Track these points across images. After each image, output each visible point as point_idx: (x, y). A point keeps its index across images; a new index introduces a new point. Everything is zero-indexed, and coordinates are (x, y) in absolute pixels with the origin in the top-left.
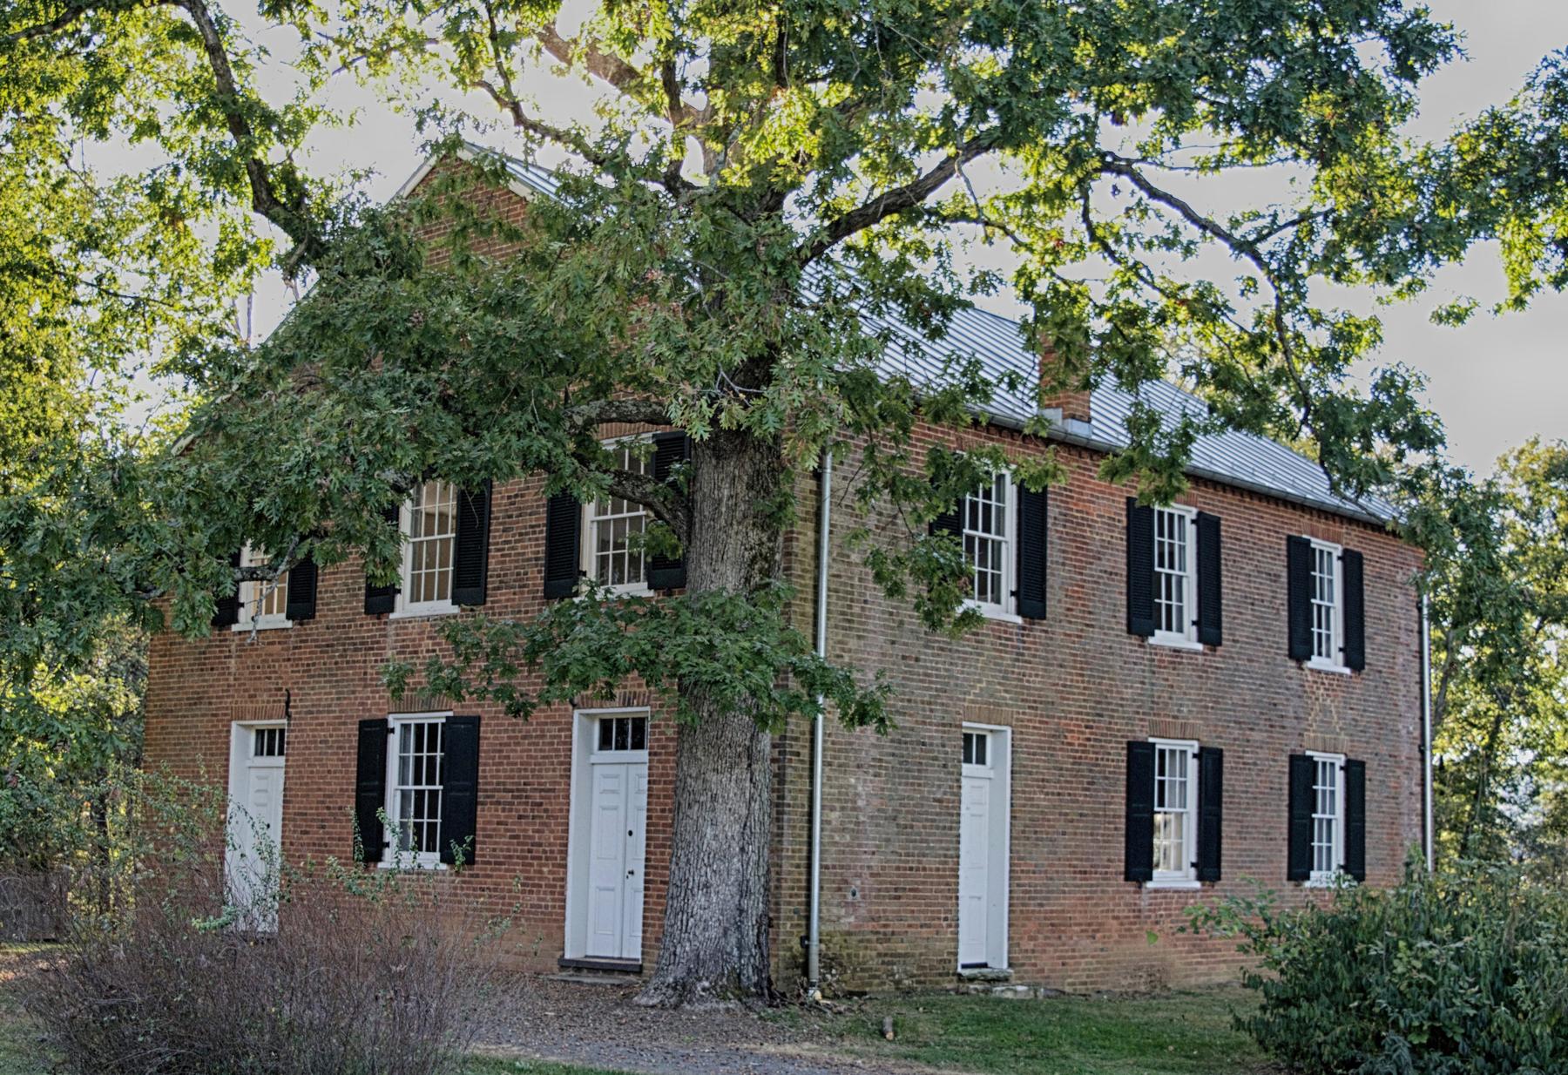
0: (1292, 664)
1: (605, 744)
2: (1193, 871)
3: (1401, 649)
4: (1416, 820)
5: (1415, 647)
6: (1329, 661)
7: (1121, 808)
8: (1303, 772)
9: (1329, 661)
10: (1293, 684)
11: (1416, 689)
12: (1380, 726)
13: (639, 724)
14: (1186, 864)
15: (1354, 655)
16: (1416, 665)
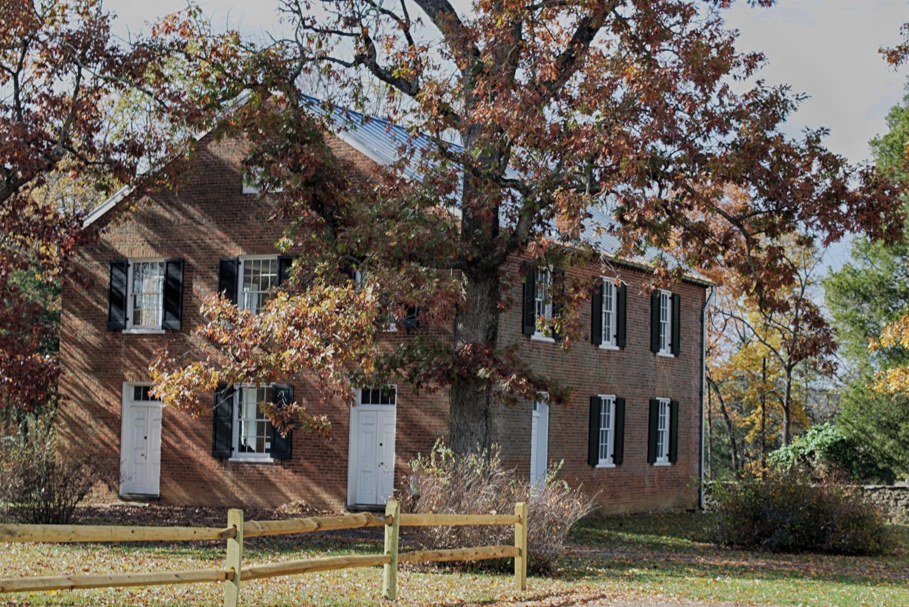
0: (652, 354)
1: (137, 398)
2: (612, 459)
3: (694, 343)
4: (697, 430)
5: (699, 342)
6: (665, 352)
7: (587, 429)
8: (654, 406)
9: (665, 352)
10: (652, 364)
11: (699, 363)
14: (608, 455)
15: (675, 347)
16: (699, 351)
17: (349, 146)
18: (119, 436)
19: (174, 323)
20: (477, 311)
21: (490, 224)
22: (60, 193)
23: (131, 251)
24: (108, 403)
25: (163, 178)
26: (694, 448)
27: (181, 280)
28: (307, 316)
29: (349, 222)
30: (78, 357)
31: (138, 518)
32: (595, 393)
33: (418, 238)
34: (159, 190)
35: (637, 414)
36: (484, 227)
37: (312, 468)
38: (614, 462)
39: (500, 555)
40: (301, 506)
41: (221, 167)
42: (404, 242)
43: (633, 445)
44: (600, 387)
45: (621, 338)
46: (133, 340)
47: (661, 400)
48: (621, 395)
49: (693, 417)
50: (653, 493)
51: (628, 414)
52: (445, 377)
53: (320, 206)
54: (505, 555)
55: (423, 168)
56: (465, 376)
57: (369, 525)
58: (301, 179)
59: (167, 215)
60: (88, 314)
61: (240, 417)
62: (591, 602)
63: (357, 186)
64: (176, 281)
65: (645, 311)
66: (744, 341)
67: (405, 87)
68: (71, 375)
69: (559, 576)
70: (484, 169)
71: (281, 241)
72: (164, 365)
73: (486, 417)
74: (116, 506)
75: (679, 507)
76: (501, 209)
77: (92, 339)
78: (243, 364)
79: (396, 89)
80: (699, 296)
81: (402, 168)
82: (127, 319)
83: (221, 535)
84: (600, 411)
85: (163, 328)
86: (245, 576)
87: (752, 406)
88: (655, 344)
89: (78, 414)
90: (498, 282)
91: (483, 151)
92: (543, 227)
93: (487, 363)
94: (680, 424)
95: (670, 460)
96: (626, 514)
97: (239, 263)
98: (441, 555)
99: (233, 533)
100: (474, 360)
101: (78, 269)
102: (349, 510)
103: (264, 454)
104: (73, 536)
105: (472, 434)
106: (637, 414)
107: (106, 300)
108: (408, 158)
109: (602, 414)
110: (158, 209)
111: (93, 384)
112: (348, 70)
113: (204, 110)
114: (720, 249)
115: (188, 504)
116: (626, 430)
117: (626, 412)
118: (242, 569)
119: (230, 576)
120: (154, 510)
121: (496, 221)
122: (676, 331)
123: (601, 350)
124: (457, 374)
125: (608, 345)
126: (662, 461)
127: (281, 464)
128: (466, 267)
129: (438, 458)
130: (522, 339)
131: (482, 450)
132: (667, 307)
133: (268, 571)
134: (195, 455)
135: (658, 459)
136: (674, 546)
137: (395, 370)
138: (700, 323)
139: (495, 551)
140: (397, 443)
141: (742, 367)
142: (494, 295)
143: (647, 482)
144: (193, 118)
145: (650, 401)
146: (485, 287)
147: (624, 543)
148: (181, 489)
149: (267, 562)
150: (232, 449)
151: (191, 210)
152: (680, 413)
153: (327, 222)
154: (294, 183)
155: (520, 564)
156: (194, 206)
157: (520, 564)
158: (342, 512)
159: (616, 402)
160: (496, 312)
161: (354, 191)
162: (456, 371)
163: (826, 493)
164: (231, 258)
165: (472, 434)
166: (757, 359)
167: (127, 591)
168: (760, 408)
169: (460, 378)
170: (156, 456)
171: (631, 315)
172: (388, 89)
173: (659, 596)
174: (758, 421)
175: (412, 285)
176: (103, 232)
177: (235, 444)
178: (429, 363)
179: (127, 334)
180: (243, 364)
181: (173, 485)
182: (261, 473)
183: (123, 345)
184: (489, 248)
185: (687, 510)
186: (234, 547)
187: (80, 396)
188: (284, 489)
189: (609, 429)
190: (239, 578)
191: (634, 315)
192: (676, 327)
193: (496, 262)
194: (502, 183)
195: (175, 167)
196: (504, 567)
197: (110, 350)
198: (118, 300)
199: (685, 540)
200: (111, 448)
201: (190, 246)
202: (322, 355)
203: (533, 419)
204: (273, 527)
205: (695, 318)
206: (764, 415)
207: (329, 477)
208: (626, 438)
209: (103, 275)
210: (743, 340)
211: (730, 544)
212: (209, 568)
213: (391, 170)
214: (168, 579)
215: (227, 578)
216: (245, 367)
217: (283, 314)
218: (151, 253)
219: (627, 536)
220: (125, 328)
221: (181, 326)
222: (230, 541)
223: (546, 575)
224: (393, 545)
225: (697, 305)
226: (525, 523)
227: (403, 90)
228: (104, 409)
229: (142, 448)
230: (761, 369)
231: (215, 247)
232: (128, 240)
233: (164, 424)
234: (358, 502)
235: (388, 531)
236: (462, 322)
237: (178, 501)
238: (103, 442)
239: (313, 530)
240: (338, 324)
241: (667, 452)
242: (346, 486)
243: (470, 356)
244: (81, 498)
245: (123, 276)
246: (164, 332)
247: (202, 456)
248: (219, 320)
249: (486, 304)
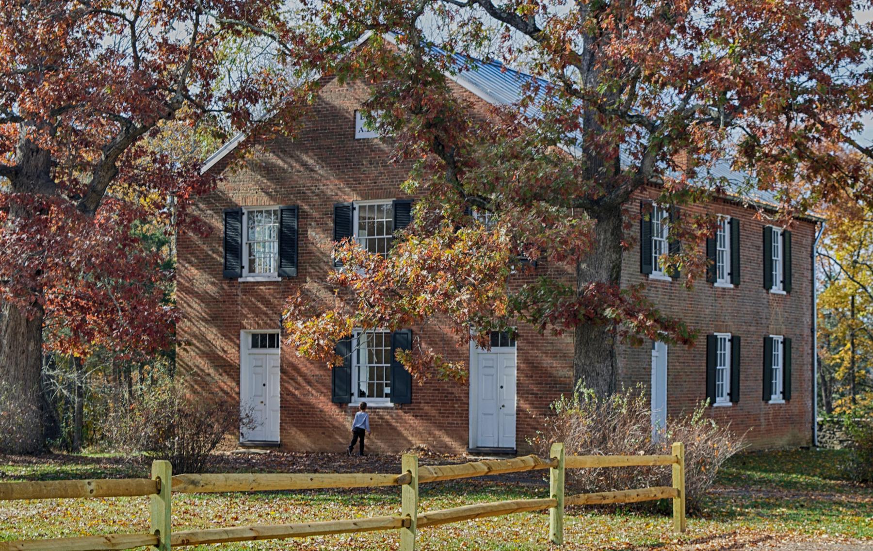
0: (765, 291)
1: (255, 345)
2: (728, 398)
3: (805, 279)
4: (810, 367)
5: (810, 278)
6: (777, 289)
7: (704, 368)
8: (768, 343)
9: (777, 289)
10: (765, 301)
11: (810, 299)
12: (797, 320)
13: (272, 336)
15: (787, 284)
16: (810, 287)
17: (462, 87)
18: (238, 384)
19: (290, 270)
20: (601, 250)
21: (612, 162)
22: (173, 141)
23: (245, 199)
24: (225, 352)
25: (278, 125)
26: (807, 385)
27: (296, 227)
28: (440, 258)
29: (472, 164)
30: (195, 306)
31: (264, 464)
32: (711, 332)
33: (546, 178)
34: (274, 136)
35: (752, 351)
36: (607, 165)
37: (434, 412)
38: (731, 401)
39: (660, 496)
40: (422, 450)
41: (335, 114)
42: (533, 182)
43: (748, 383)
44: (716, 325)
45: (735, 276)
46: (249, 288)
47: (775, 337)
48: (737, 334)
49: (805, 353)
50: (769, 431)
51: (743, 352)
52: (573, 318)
53: (440, 148)
54: (665, 496)
55: (548, 107)
56: (592, 316)
57: (536, 468)
58: (422, 121)
59: (280, 163)
60: (205, 263)
61: (358, 362)
62: (761, 544)
63: (477, 126)
64: (291, 229)
65: (758, 248)
66: (830, 279)
67: (521, 26)
68: (189, 324)
69: (709, 517)
70: (610, 106)
71: (406, 183)
72: (297, 312)
73: (612, 357)
74: (237, 454)
75: (794, 444)
76: (623, 146)
77: (211, 289)
78: (377, 309)
79: (512, 28)
80: (809, 232)
81: (526, 106)
82: (243, 267)
83: (396, 481)
84: (716, 350)
85: (279, 276)
86: (420, 523)
87: (840, 343)
88: (768, 283)
89: (197, 364)
90: (621, 220)
91: (609, 87)
92: (667, 163)
93: (614, 302)
94: (793, 361)
95: (784, 398)
96: (743, 453)
97: (354, 209)
98: (604, 498)
99: (408, 478)
100: (599, 300)
101: (196, 220)
102: (471, 454)
103: (384, 399)
104: (254, 485)
105: (598, 374)
106: (752, 351)
107: (221, 249)
108: (533, 95)
109: (719, 352)
110: (272, 158)
111: (212, 334)
112: (462, 11)
113: (327, 52)
114: (850, 182)
115: (309, 450)
116: (742, 369)
118: (419, 515)
119: (406, 524)
120: (277, 457)
121: (618, 160)
122: (787, 268)
123: (716, 288)
124: (584, 315)
125: (724, 282)
126: (777, 398)
127: (401, 409)
128: (589, 206)
129: (581, 400)
130: (642, 279)
131: (627, 389)
132: (779, 243)
133: (443, 517)
134: (314, 401)
135: (773, 397)
136: (807, 484)
137: (519, 312)
138: (810, 260)
139: (655, 492)
141: (830, 305)
142: (617, 234)
143: (763, 421)
144: (315, 59)
145: (765, 339)
146: (608, 226)
147: (755, 483)
148: (302, 435)
149: (436, 508)
150: (352, 394)
151: (305, 158)
152: (793, 351)
153: (448, 163)
154: (416, 123)
155: (678, 505)
156: (307, 153)
157: (678, 505)
158: (464, 455)
159: (731, 341)
160: (619, 250)
161: (474, 132)
162: (583, 312)
164: (346, 204)
165: (598, 374)
166: (846, 295)
167: (291, 540)
168: (849, 345)
169: (586, 319)
170: (276, 402)
171: (744, 253)
172: (503, 30)
173: (824, 536)
174: (847, 357)
175: (544, 225)
176: (221, 180)
177: (355, 390)
178: (554, 304)
179: (244, 283)
180: (377, 309)
181: (293, 431)
182: (382, 418)
183: (239, 293)
184: (612, 186)
185: (802, 448)
186: (409, 493)
187: (198, 344)
188: (405, 433)
189: (725, 368)
190: (415, 526)
191: (747, 253)
192: (787, 263)
193: (620, 200)
194: (627, 118)
195: (291, 112)
196: (663, 509)
197: (230, 298)
198: (232, 248)
199: (816, 478)
200: (231, 396)
201: (304, 193)
202: (457, 299)
203: (653, 359)
204: (448, 472)
205: (805, 254)
206: (853, 352)
207: (450, 420)
208: (742, 377)
209: (218, 224)
210: (829, 277)
211: (865, 481)
212: (391, 514)
213: (514, 109)
214: (347, 528)
215: (403, 525)
216: (378, 312)
217: (416, 257)
218: (265, 199)
219: (757, 475)
222: (405, 487)
223: (696, 515)
224: (559, 489)
225: (807, 241)
226: (683, 463)
227: (518, 28)
228: (222, 357)
229: (261, 396)
230: (850, 306)
231: (329, 193)
232: (243, 189)
233: (283, 371)
234: (479, 445)
235: (553, 474)
236: (584, 261)
237: (298, 447)
238: (222, 390)
239: (483, 474)
240: (472, 266)
241: (781, 390)
242: (467, 429)
243: (594, 296)
244: (213, 446)
245: (239, 225)
246: (280, 279)
247: (324, 404)
248: (351, 265)
249: (609, 243)
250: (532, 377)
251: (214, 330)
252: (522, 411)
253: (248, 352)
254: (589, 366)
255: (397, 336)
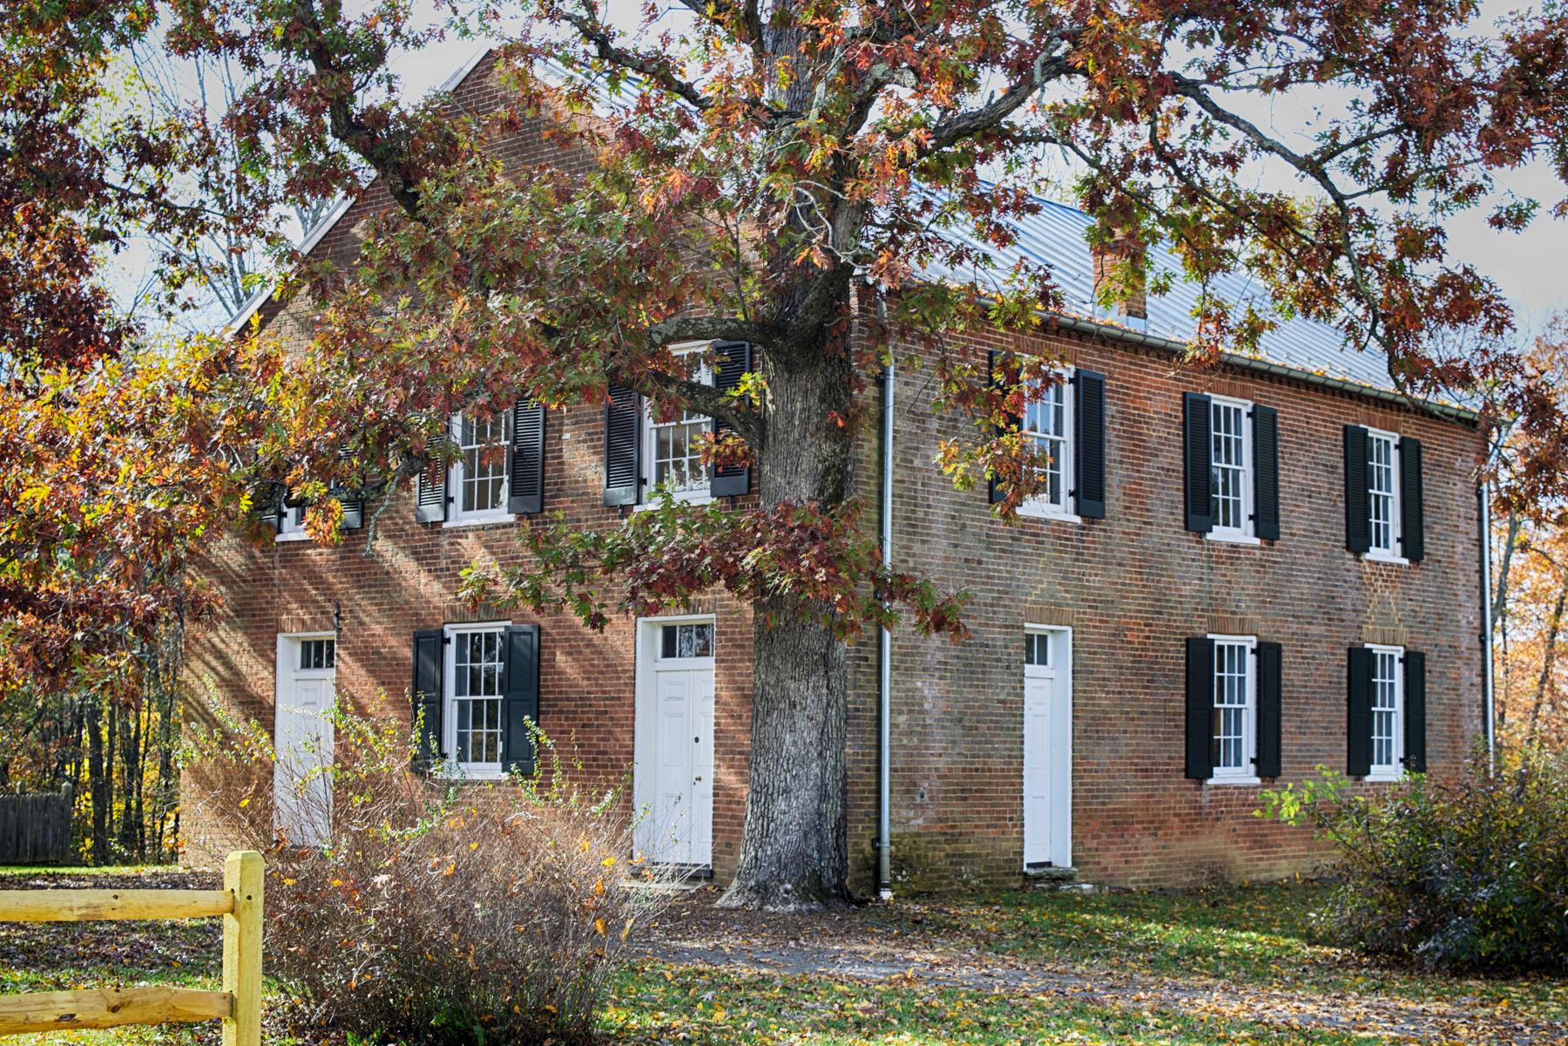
2: (1252, 767)
4: (1477, 711)
5: (1475, 536)
8: (1361, 665)
10: (1351, 577)
11: (1476, 578)
12: (1440, 616)
14: (1245, 760)
15: (1413, 545)
16: (1476, 554)
32: (1200, 632)
35: (1314, 675)
38: (1258, 774)
45: (1267, 522)
49: (1465, 684)
117: (1285, 671)
138: (1475, 500)
140: (719, 733)
145: (1350, 650)
163: (46, 681)
171: (1290, 478)
197: (259, 576)
220: (280, 531)
221: (363, 521)
250: (740, 717)
251: (240, 637)
252: (722, 788)
253: (294, 676)
254: (774, 687)
255: (515, 638)
